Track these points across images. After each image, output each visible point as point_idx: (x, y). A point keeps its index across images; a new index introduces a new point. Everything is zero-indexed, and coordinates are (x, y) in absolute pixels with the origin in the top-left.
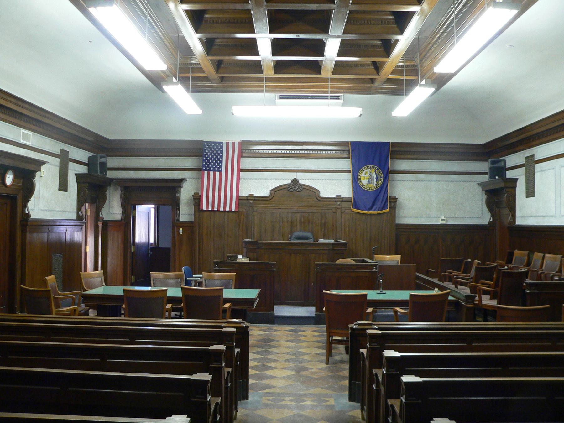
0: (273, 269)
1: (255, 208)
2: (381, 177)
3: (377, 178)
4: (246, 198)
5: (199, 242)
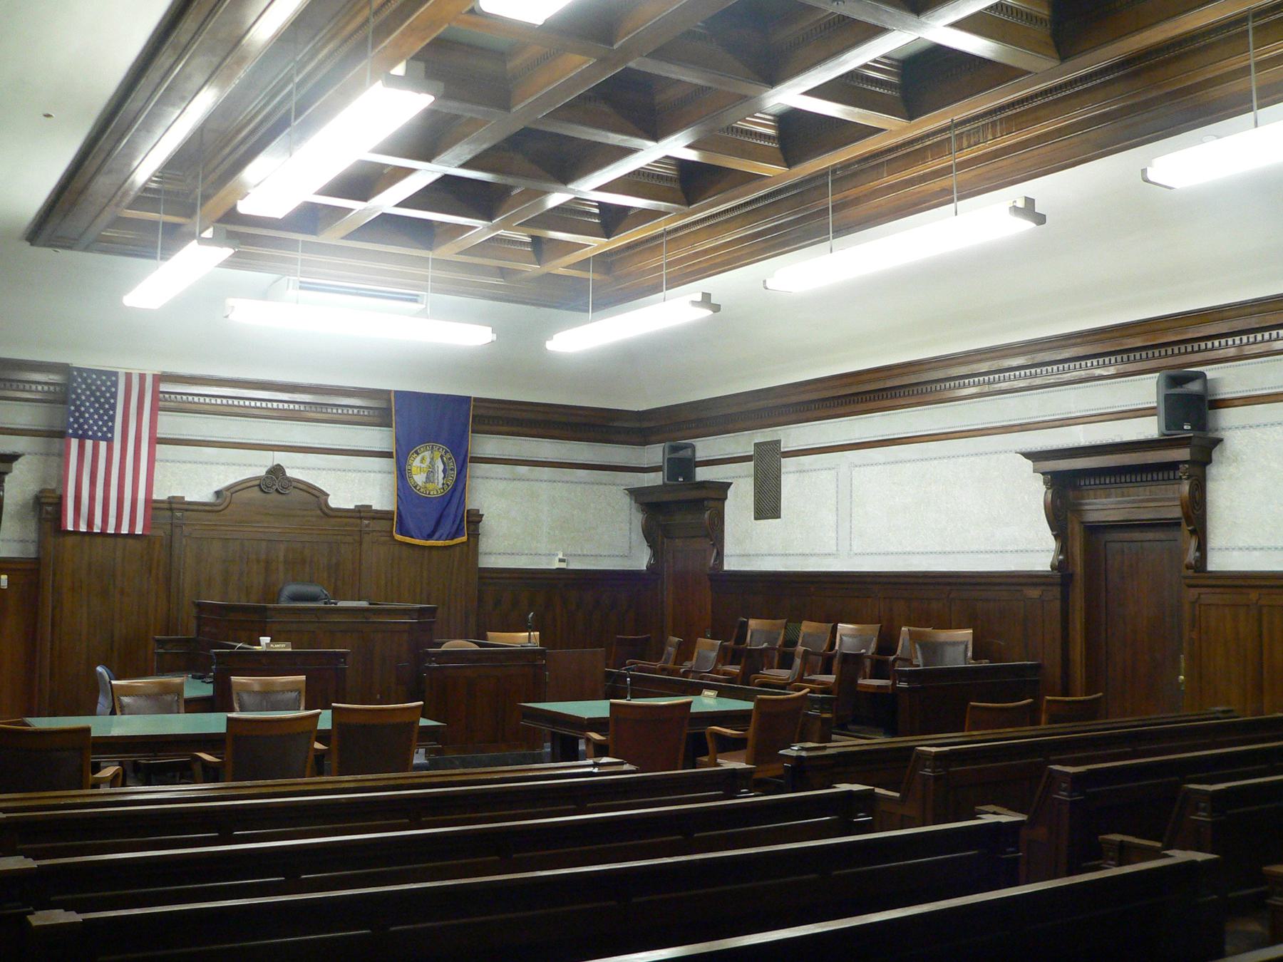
3: (444, 471)
5: (54, 608)
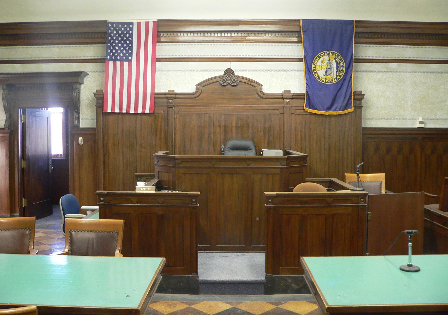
0: (194, 205)
1: (176, 109)
2: (343, 66)
3: (337, 68)
4: (164, 96)
